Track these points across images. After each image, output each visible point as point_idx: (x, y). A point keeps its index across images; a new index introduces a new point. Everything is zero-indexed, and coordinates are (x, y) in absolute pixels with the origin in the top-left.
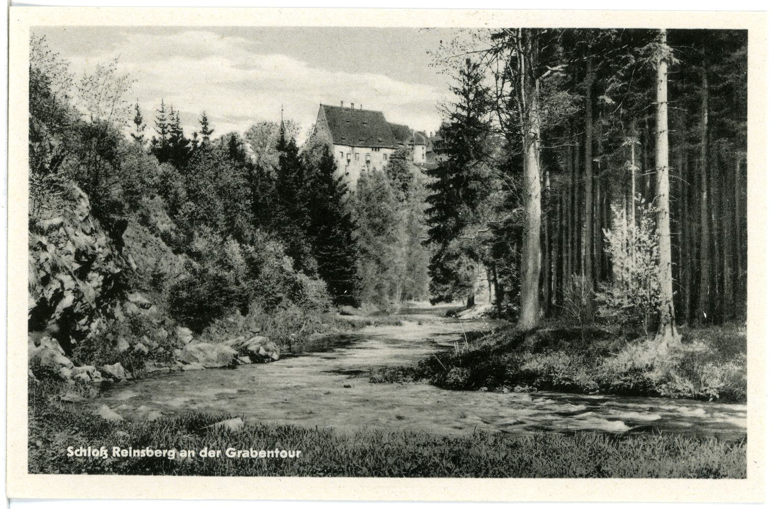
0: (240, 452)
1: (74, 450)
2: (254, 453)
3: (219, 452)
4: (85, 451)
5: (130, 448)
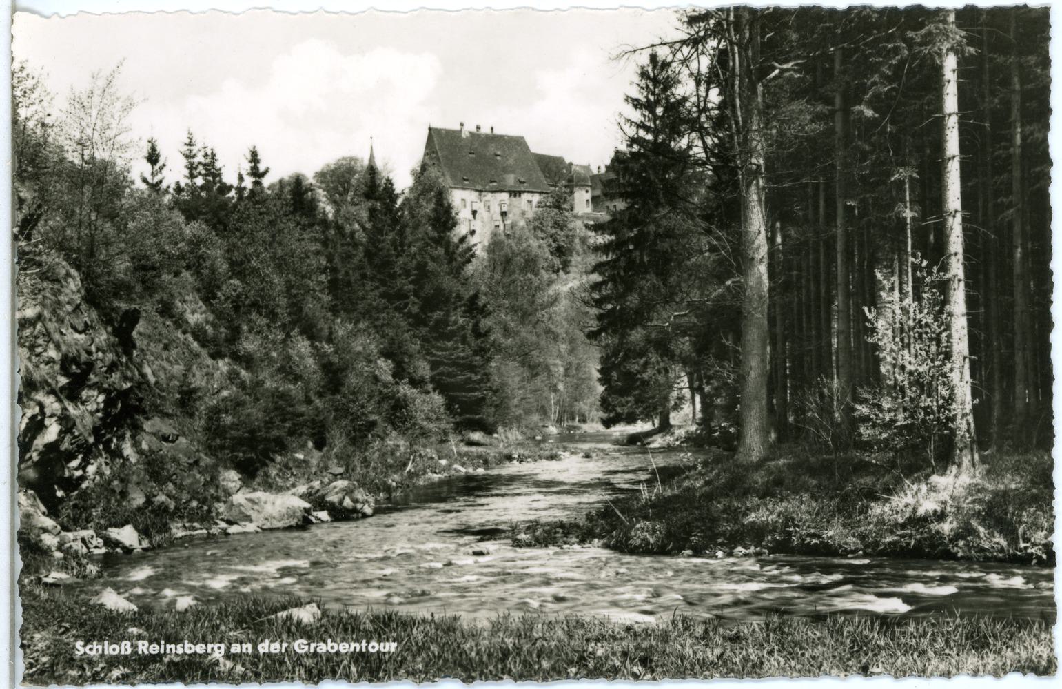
0: (313, 645)
1: (84, 646)
2: (332, 648)
3: (249, 646)
4: (100, 647)
5: (106, 643)
